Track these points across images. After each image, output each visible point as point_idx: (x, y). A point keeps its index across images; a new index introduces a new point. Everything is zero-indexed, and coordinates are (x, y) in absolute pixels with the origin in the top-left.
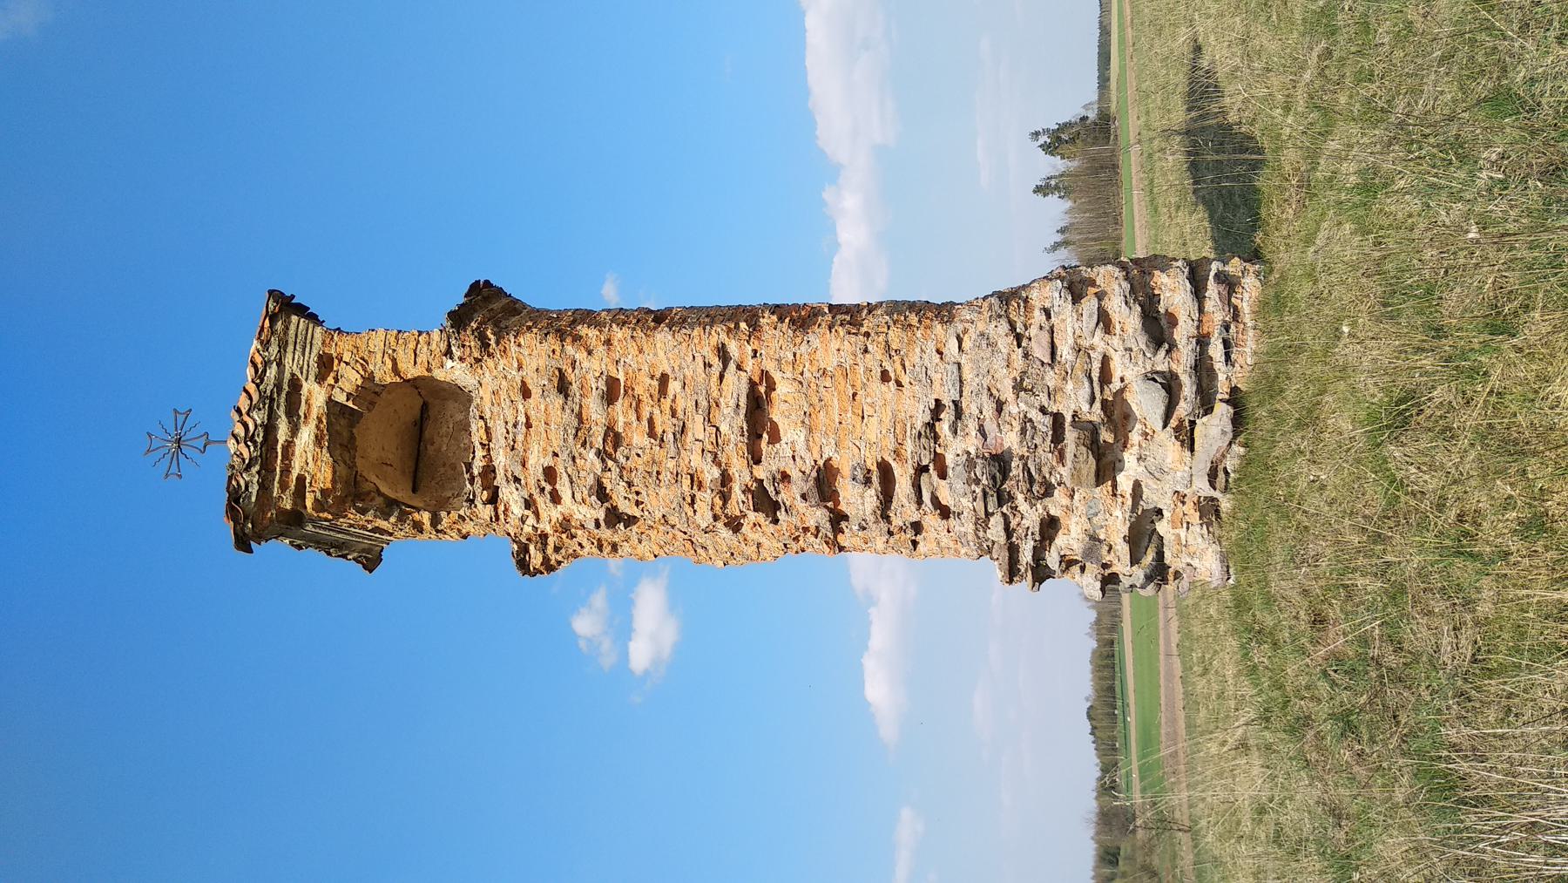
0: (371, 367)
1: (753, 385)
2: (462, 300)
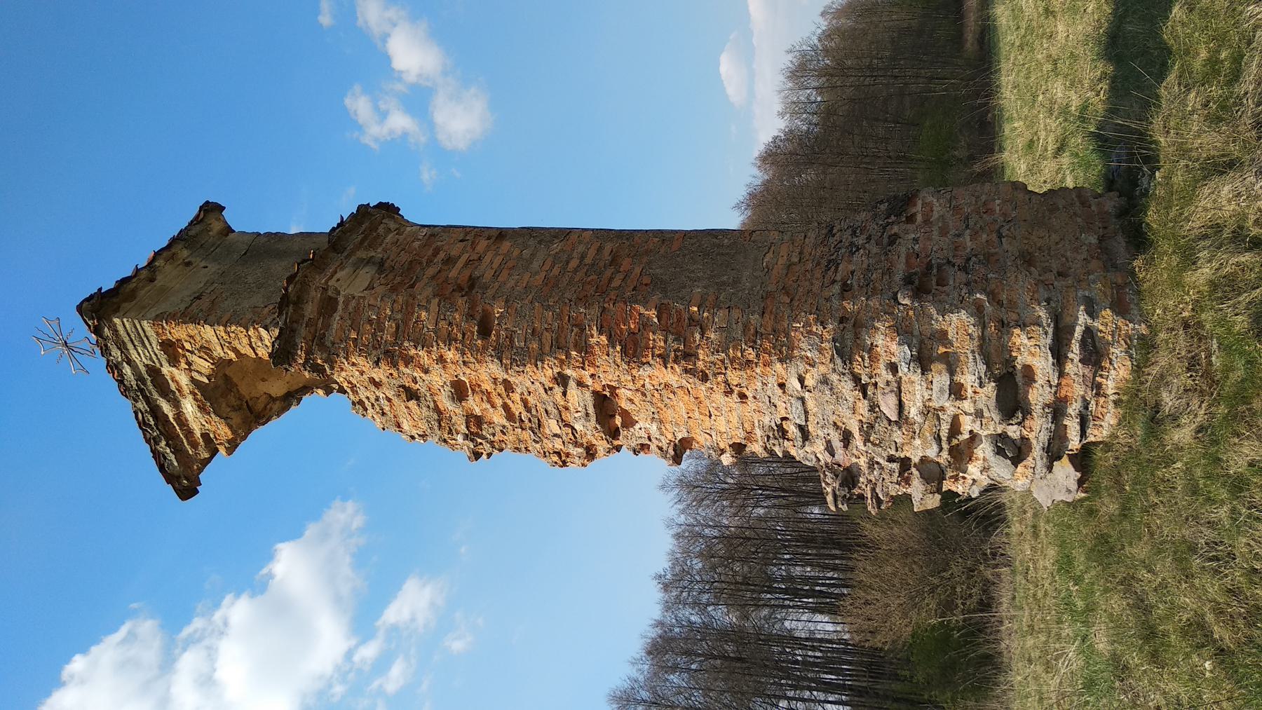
1: (595, 393)
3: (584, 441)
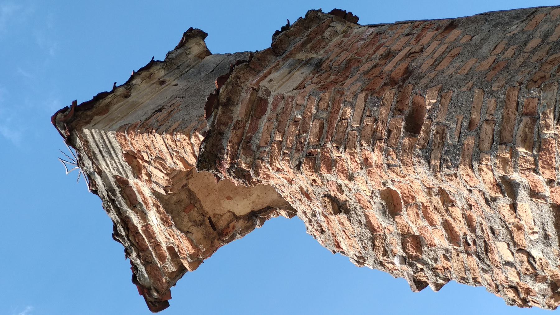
3: (548, 273)
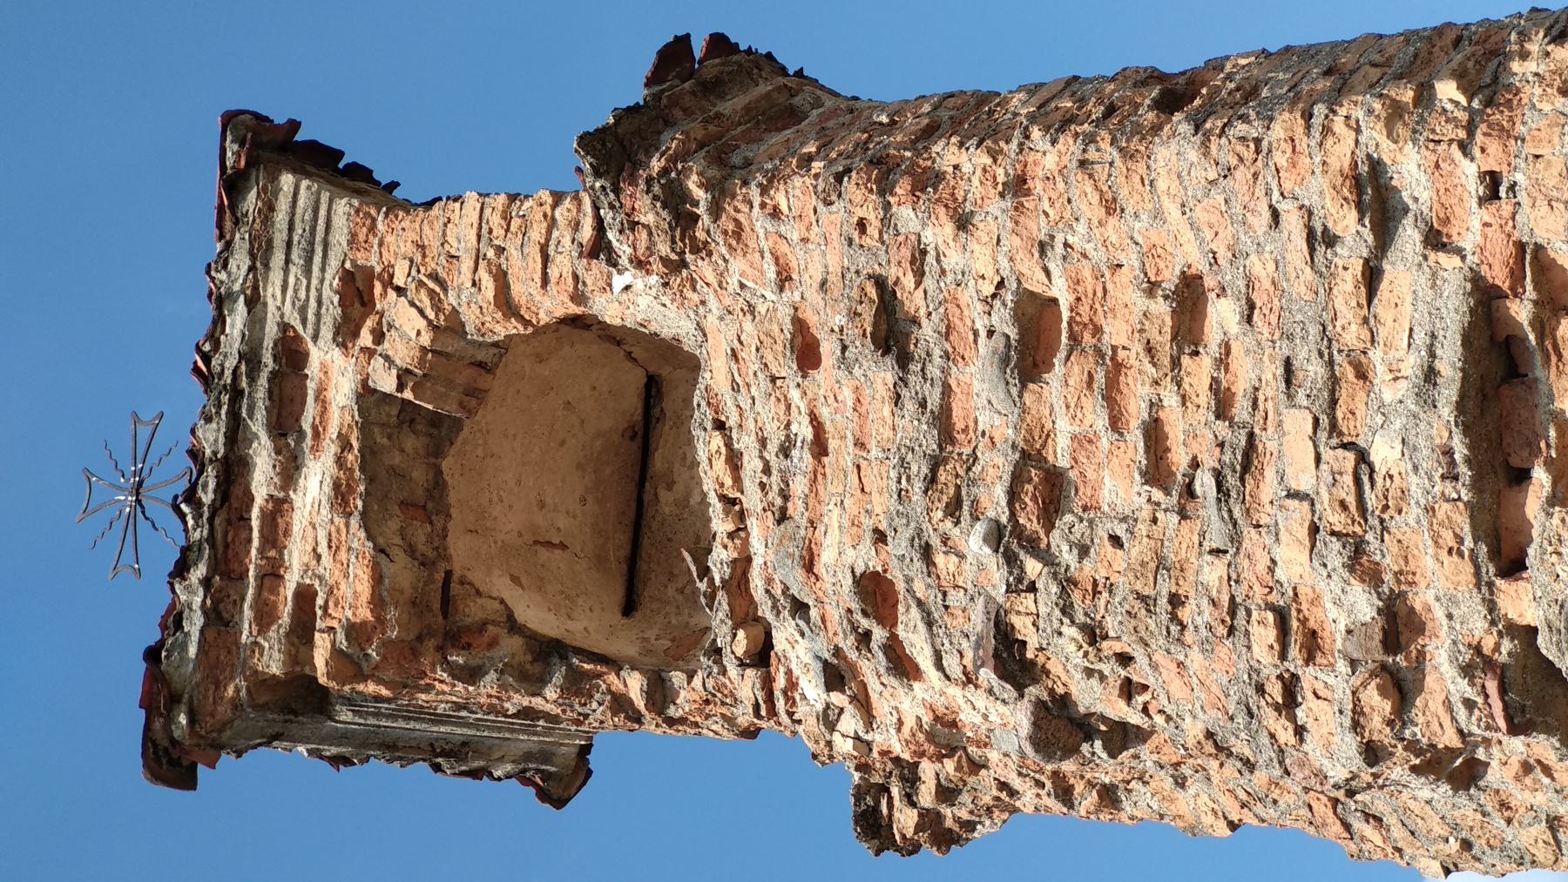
0: (452, 298)
1: (1485, 300)
2: (637, 94)
